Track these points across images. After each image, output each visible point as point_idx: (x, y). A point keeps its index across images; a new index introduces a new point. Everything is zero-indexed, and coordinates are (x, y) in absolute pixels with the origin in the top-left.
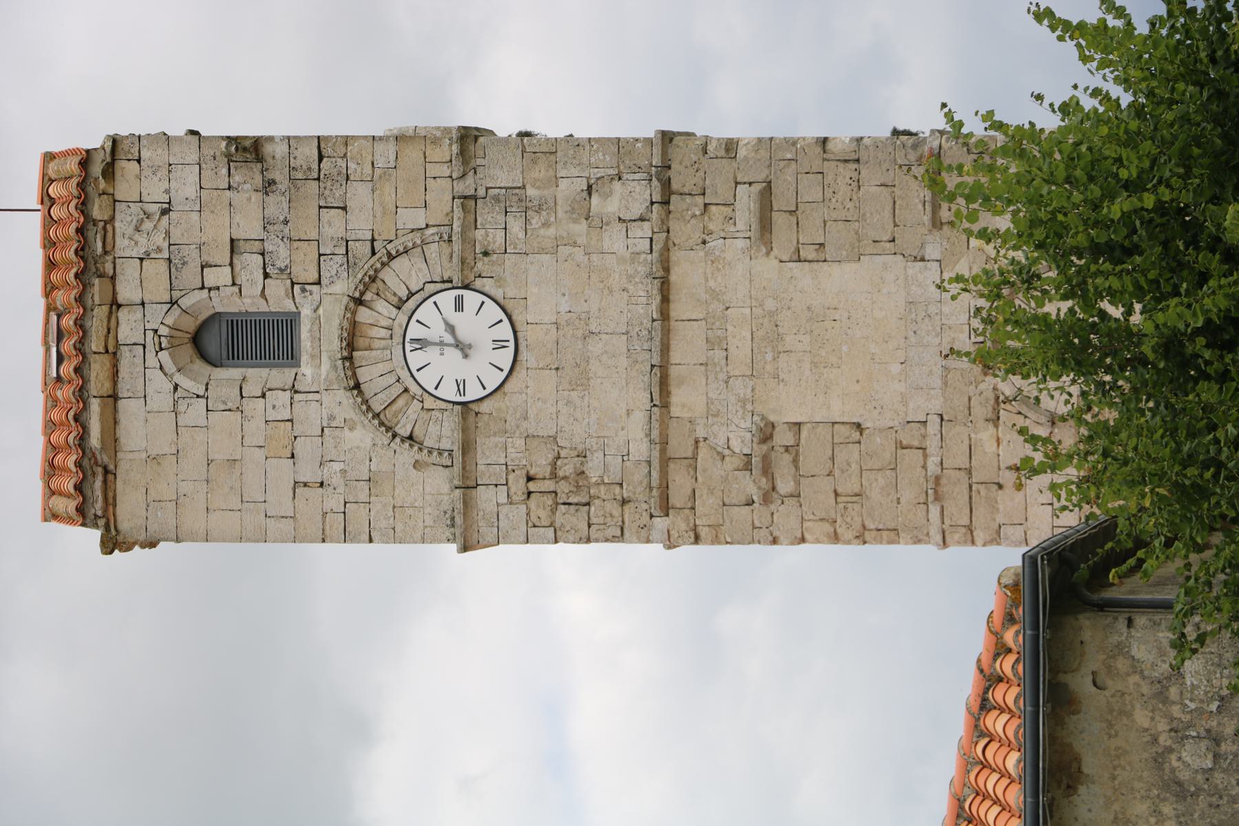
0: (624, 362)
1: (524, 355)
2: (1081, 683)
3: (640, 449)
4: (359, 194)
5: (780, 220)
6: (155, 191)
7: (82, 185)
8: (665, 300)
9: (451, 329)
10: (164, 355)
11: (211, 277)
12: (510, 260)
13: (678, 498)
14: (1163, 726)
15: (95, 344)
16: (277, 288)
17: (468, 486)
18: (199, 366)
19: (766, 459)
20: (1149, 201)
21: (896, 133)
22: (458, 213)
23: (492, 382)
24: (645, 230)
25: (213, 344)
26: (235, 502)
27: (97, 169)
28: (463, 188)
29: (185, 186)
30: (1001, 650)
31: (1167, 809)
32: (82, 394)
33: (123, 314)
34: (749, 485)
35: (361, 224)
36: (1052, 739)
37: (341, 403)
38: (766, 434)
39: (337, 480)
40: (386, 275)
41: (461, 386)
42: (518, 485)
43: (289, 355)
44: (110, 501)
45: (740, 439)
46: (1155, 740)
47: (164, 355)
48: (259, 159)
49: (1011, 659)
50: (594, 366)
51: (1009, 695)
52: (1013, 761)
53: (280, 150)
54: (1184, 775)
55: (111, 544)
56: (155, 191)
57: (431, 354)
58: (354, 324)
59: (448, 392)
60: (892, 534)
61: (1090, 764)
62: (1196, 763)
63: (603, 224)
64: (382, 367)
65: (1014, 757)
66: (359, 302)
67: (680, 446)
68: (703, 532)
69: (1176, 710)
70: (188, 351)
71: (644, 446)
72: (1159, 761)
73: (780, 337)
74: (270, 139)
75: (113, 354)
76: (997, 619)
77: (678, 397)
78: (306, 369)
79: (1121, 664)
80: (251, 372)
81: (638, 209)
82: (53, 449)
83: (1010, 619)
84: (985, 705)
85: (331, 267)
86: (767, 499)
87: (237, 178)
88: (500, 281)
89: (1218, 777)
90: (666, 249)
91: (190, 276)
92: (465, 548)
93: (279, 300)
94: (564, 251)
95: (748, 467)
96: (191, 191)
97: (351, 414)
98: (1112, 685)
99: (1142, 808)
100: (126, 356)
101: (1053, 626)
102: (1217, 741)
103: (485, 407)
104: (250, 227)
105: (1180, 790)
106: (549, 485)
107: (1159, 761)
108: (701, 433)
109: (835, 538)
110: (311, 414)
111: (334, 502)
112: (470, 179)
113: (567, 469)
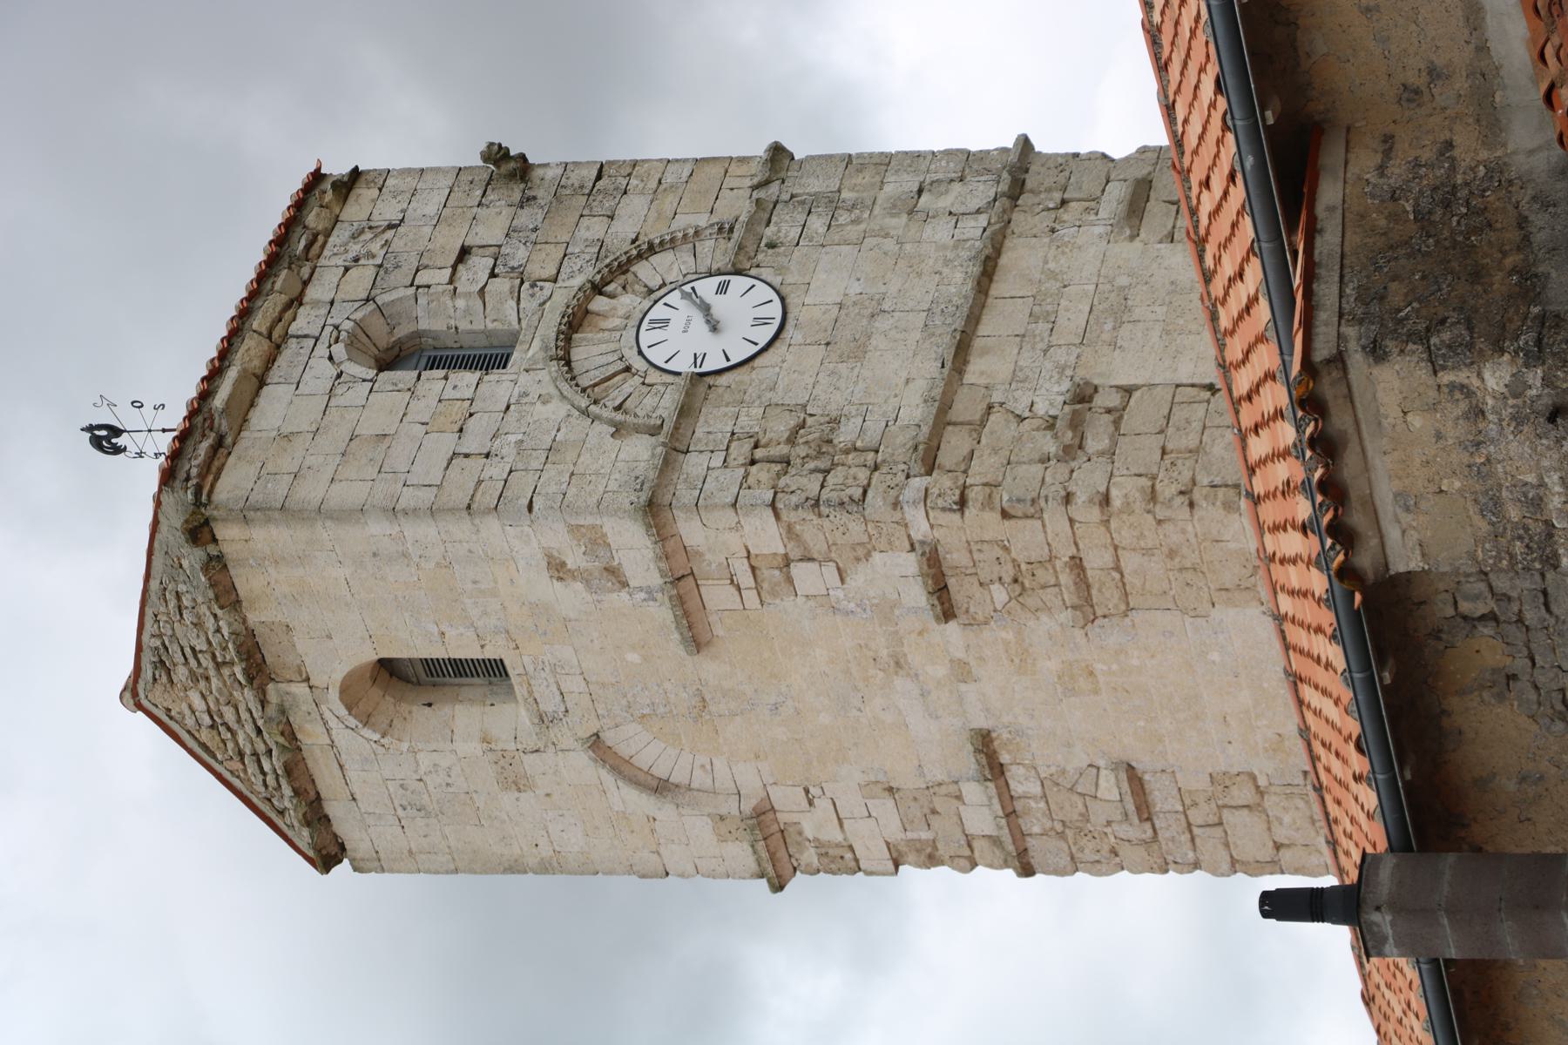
38: (1083, 396)
67: (966, 407)
88: (780, 270)
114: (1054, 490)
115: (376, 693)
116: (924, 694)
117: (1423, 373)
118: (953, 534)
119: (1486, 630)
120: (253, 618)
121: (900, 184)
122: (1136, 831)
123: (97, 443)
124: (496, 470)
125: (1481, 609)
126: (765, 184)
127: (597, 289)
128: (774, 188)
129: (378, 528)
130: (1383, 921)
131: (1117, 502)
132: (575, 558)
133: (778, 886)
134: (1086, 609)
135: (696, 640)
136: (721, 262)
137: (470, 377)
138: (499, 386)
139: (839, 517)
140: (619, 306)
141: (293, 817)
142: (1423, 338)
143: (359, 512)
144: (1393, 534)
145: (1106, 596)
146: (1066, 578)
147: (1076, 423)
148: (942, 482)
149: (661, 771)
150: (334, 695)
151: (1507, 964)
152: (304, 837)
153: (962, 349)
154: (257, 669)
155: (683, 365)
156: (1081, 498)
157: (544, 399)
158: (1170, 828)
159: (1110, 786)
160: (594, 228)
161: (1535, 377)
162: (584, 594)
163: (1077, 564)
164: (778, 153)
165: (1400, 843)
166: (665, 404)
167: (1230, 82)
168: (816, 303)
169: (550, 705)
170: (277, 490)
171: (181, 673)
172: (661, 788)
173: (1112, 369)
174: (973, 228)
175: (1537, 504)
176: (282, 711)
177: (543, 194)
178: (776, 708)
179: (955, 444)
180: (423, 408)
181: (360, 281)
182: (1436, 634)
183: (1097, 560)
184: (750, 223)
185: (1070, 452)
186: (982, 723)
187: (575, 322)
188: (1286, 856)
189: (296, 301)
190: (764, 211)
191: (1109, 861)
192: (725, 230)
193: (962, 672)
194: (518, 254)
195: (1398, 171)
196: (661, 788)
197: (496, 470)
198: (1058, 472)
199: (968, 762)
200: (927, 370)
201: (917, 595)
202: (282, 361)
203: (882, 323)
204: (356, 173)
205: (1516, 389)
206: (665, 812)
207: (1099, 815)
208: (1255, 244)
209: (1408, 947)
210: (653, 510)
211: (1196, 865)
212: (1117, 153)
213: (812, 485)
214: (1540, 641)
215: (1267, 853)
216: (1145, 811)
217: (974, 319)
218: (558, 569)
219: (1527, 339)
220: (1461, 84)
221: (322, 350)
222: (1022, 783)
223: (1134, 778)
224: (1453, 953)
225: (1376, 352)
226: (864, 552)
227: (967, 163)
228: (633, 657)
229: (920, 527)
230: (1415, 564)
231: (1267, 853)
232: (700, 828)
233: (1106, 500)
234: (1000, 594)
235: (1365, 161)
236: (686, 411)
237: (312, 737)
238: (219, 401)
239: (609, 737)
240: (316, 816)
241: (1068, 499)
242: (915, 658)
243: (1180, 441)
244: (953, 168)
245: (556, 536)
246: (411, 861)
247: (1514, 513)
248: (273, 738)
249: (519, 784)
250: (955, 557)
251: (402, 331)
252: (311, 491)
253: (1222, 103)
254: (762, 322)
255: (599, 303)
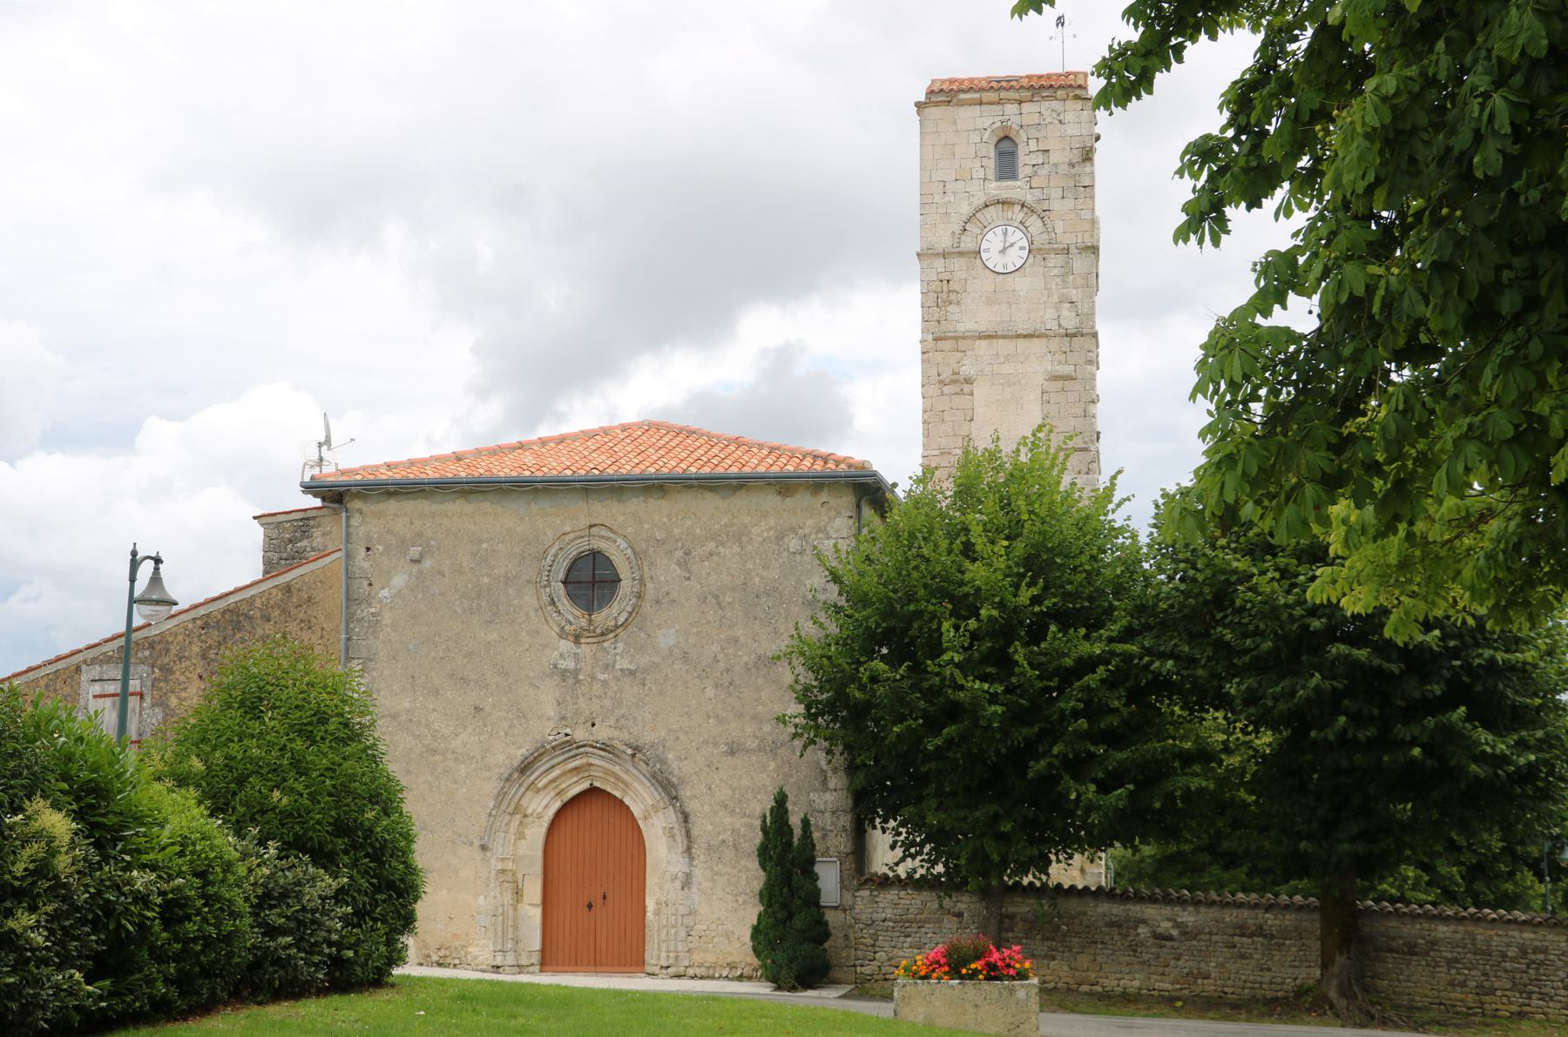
0: (998, 319)
1: (1001, 277)
2: (824, 496)
3: (961, 328)
4: (1069, 204)
5: (1060, 384)
6: (1069, 117)
7: (1070, 86)
8: (1025, 336)
9: (1012, 245)
10: (999, 124)
11: (1033, 143)
12: (1041, 269)
13: (941, 344)
14: (806, 531)
15: (1003, 94)
16: (1028, 170)
17: (944, 255)
18: (995, 139)
19: (956, 381)
20: (1025, 517)
21: (1098, 433)
22: (1061, 246)
23: (990, 264)
24: (1054, 327)
25: (1005, 145)
26: (936, 157)
27: (1078, 92)
28: (1073, 250)
29: (1072, 130)
30: (837, 463)
31: (772, 533)
32: (982, 90)
33: (1016, 105)
34: (946, 374)
35: (1056, 205)
36: (800, 485)
37: (979, 200)
38: (968, 381)
39: (947, 199)
40: (1035, 216)
41: (987, 250)
42: (945, 276)
43: (1000, 178)
44: (937, 104)
45: (967, 369)
46: (800, 528)
47: (999, 124)
48: (1084, 161)
49: (833, 467)
50: (997, 307)
51: (818, 467)
52: (790, 468)
53: (1088, 169)
54: (786, 540)
55: (919, 105)
56: (1069, 117)
57: (1001, 237)
58: (1013, 204)
59: (984, 245)
60: (927, 435)
61: (789, 500)
62: (791, 545)
63: (1057, 309)
64: (995, 217)
65: (792, 469)
66: (1023, 206)
67: (963, 344)
68: (926, 356)
69: (813, 536)
70: (1002, 134)
71: (963, 329)
72: (792, 529)
73: (1009, 386)
74: (1092, 165)
75: (999, 102)
76: (850, 461)
77: (983, 343)
78: (994, 184)
79: (833, 513)
80: (993, 161)
81: (1064, 323)
82: (962, 81)
83: (850, 466)
84: (815, 457)
85: (1037, 193)
86: (940, 382)
87: (1075, 152)
88: (1032, 265)
89: (785, 554)
90: (1047, 336)
91: (1033, 133)
92: (918, 255)
93: (1023, 171)
94: (1046, 292)
95: (954, 373)
96: (1069, 132)
97: (975, 204)
98: (824, 510)
99: (772, 523)
100: (999, 107)
101: (847, 484)
102: (800, 553)
103: (978, 261)
104: (1054, 157)
105: (779, 538)
106: (945, 289)
107: (792, 529)
108: (968, 353)
109: (925, 411)
110: (975, 187)
111: (937, 198)
112: (1076, 251)
113: (953, 297)
162: (612, 551)
208: (540, 785)
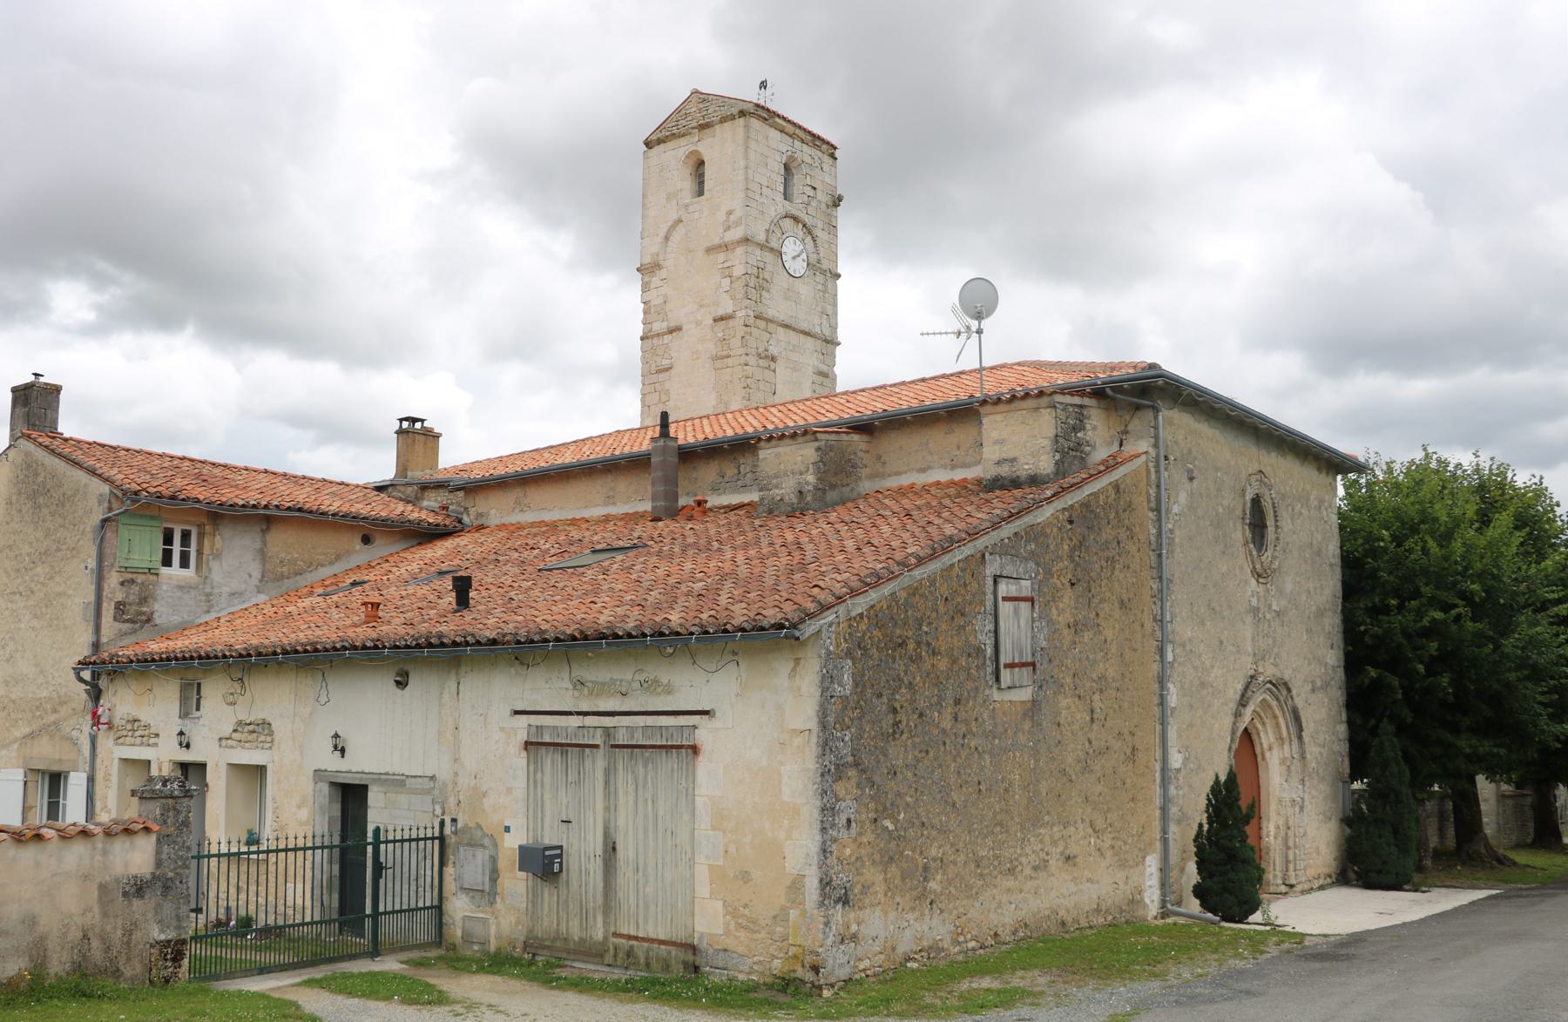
38: (773, 359)
67: (771, 327)
114: (749, 351)
115: (695, 159)
116: (692, 313)
117: (812, 461)
118: (737, 323)
119: (736, 471)
120: (717, 127)
121: (829, 310)
122: (653, 369)
123: (762, 82)
124: (757, 197)
125: (742, 470)
126: (831, 273)
127: (804, 226)
128: (829, 275)
129: (742, 163)
130: (661, 443)
131: (745, 368)
132: (732, 218)
133: (638, 270)
134: (716, 358)
135: (709, 250)
136: (811, 260)
137: (782, 189)
138: (780, 198)
139: (743, 291)
140: (800, 232)
141: (660, 135)
142: (821, 461)
143: (746, 158)
144: (769, 451)
145: (719, 364)
146: (724, 353)
147: (767, 357)
148: (752, 320)
149: (671, 238)
150: (695, 148)
151: (650, 474)
152: (654, 137)
153: (786, 326)
154: (703, 127)
155: (784, 249)
156: (747, 358)
157: (776, 210)
158: (655, 378)
159: (666, 362)
160: (820, 225)
161: (811, 488)
163: (729, 356)
164: (838, 276)
165: (680, 448)
166: (774, 244)
167: (886, 413)
168: (798, 283)
169: (691, 209)
170: (753, 135)
171: (701, 106)
172: (667, 238)
173: (780, 367)
174: (817, 330)
175: (777, 487)
176: (690, 133)
177: (829, 211)
178: (689, 271)
179: (762, 324)
180: (774, 176)
181: (808, 159)
182: (735, 459)
183: (729, 361)
184: (820, 268)
185: (759, 355)
186: (684, 328)
187: (796, 219)
188: (646, 408)
189: (803, 142)
190: (823, 272)
191: (645, 361)
192: (819, 261)
193: (699, 323)
194: (814, 204)
195: (860, 454)
196: (667, 238)
197: (757, 197)
198: (754, 351)
199: (673, 324)
200: (781, 317)
201: (721, 312)
202: (787, 137)
203: (793, 304)
204: (836, 159)
205: (807, 483)
206: (659, 239)
207: (659, 359)
209: (654, 448)
210: (746, 240)
211: (643, 384)
212: (835, 369)
213: (752, 285)
214: (733, 484)
215: (647, 403)
216: (658, 372)
217: (794, 330)
218: (730, 213)
219: (820, 486)
220: (881, 470)
221: (790, 148)
222: (667, 338)
223: (667, 369)
224: (652, 460)
225: (818, 449)
226: (733, 298)
227: (834, 328)
228: (704, 232)
229: (739, 314)
230: (761, 456)
231: (647, 403)
232: (655, 249)
233: (746, 365)
234: (720, 335)
235: (863, 446)
236: (772, 250)
237: (683, 141)
238: (777, 120)
239: (681, 224)
240: (660, 141)
241: (747, 354)
242: (702, 311)
243: (761, 385)
244: (833, 324)
245: (739, 213)
246: (646, 168)
247: (774, 481)
248: (683, 130)
249: (668, 199)
250: (731, 323)
251: (793, 170)
252: (753, 145)
253: (880, 411)
254: (795, 271)
255: (801, 226)
